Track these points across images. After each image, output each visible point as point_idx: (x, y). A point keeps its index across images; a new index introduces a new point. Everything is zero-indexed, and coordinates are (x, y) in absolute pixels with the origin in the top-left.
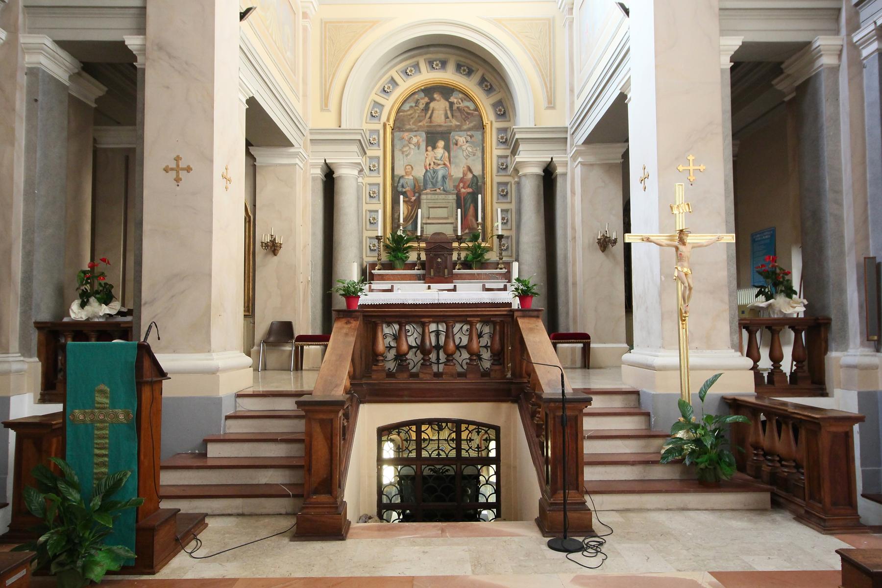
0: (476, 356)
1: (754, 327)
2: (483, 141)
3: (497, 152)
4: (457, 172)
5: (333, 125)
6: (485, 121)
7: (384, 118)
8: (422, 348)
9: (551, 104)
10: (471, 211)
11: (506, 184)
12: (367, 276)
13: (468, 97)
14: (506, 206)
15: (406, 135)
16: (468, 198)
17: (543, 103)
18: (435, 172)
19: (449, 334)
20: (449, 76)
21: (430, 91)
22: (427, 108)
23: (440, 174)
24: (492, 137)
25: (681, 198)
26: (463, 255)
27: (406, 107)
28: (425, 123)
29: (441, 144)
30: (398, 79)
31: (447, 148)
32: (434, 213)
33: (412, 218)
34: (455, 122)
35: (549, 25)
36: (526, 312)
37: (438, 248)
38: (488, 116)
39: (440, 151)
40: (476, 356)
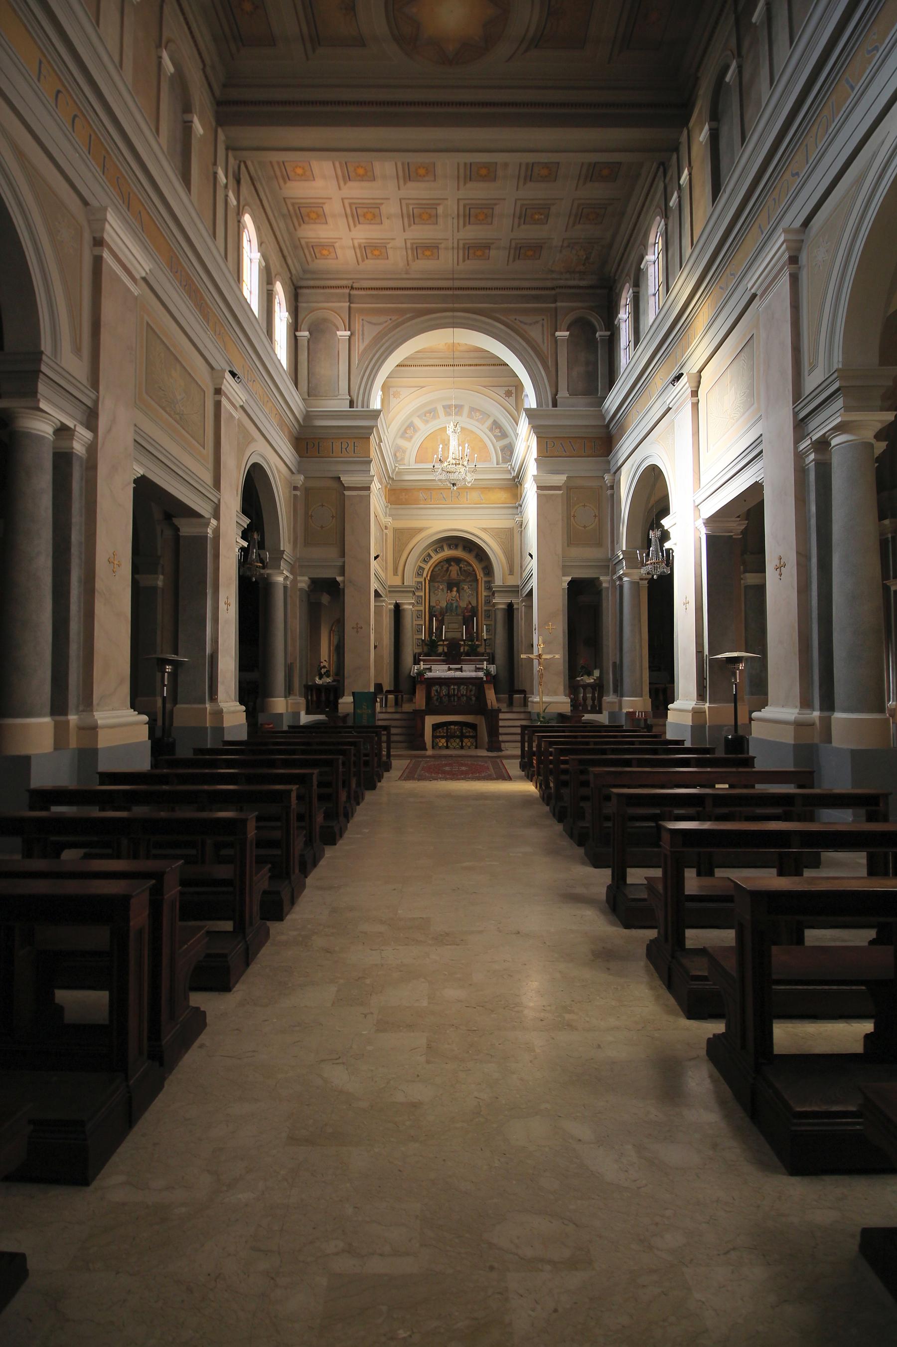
0: (469, 698)
1: (573, 688)
2: (477, 588)
3: (484, 594)
4: (463, 604)
5: (400, 583)
6: (479, 577)
7: (425, 575)
8: (448, 695)
9: (511, 572)
10: (470, 626)
11: (489, 610)
12: (416, 662)
13: (469, 564)
14: (488, 623)
15: (436, 584)
16: (469, 617)
17: (507, 572)
18: (452, 604)
19: (459, 690)
20: (458, 553)
21: (449, 561)
22: (447, 569)
23: (454, 605)
24: (482, 587)
25: (545, 643)
26: (466, 648)
27: (437, 569)
28: (446, 578)
29: (455, 589)
30: (432, 554)
31: (458, 591)
32: (451, 626)
33: (439, 629)
34: (462, 578)
35: (510, 531)
36: (487, 682)
37: (454, 645)
38: (480, 575)
39: (454, 593)
40: (469, 698)
